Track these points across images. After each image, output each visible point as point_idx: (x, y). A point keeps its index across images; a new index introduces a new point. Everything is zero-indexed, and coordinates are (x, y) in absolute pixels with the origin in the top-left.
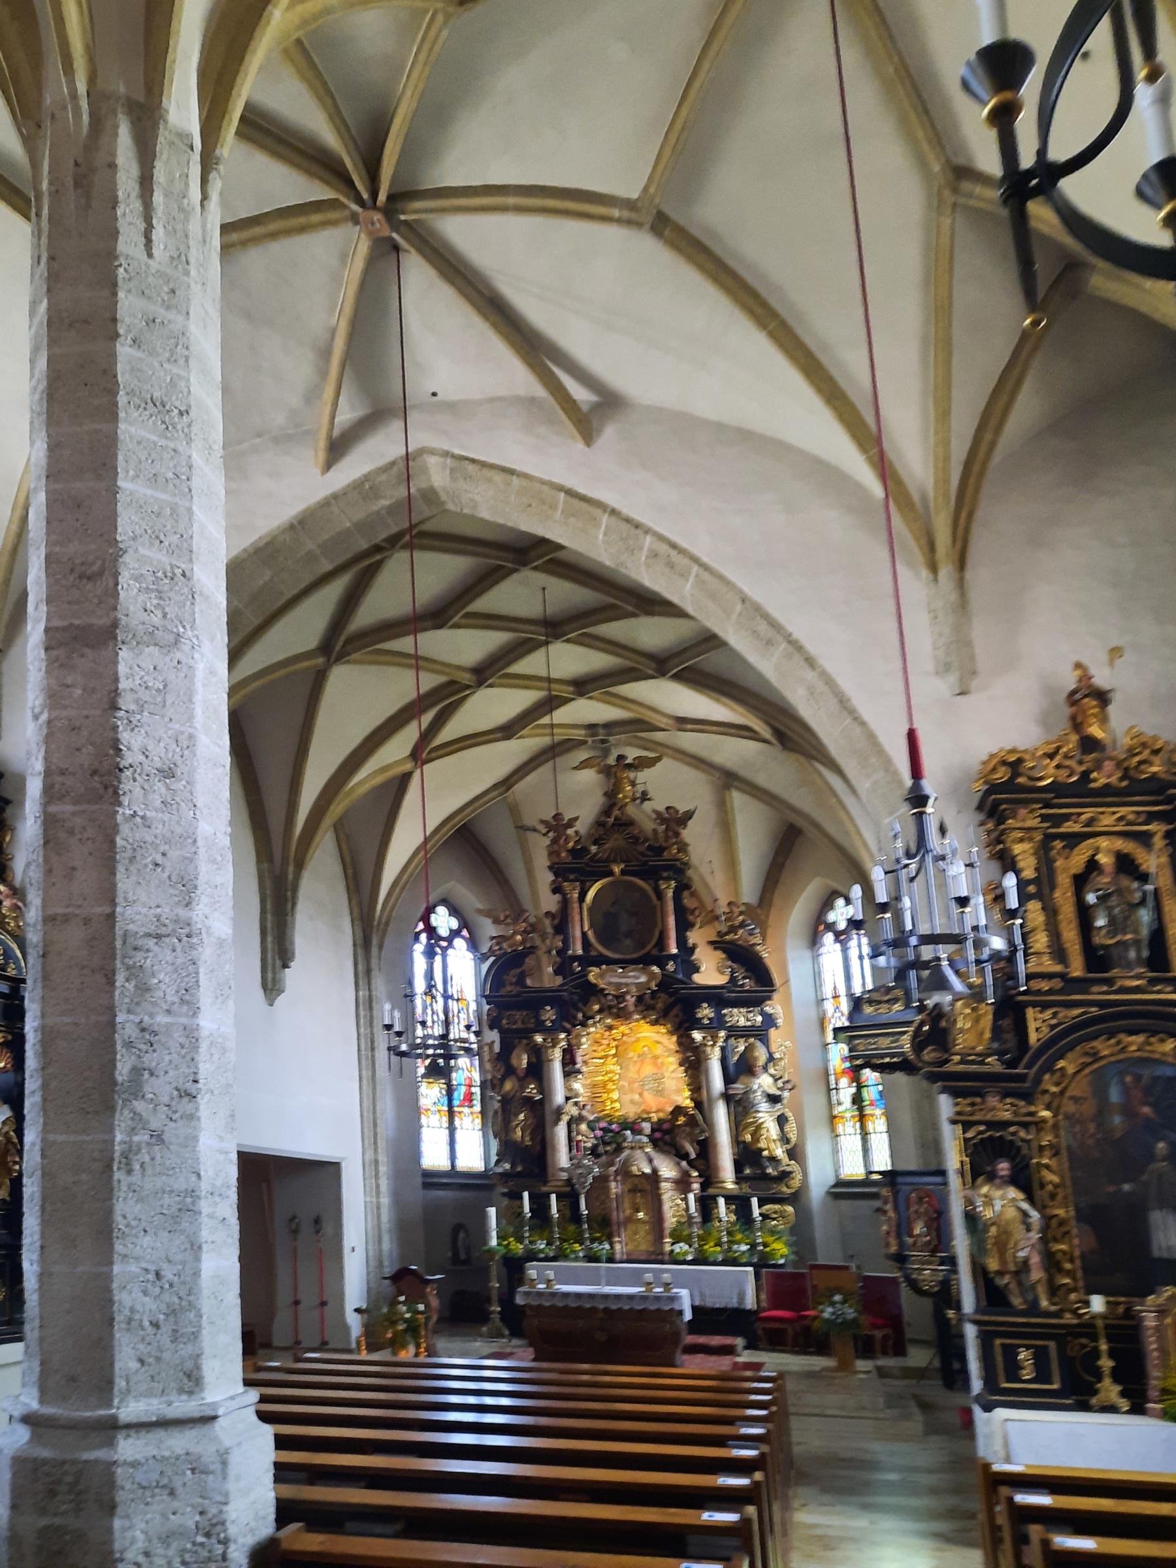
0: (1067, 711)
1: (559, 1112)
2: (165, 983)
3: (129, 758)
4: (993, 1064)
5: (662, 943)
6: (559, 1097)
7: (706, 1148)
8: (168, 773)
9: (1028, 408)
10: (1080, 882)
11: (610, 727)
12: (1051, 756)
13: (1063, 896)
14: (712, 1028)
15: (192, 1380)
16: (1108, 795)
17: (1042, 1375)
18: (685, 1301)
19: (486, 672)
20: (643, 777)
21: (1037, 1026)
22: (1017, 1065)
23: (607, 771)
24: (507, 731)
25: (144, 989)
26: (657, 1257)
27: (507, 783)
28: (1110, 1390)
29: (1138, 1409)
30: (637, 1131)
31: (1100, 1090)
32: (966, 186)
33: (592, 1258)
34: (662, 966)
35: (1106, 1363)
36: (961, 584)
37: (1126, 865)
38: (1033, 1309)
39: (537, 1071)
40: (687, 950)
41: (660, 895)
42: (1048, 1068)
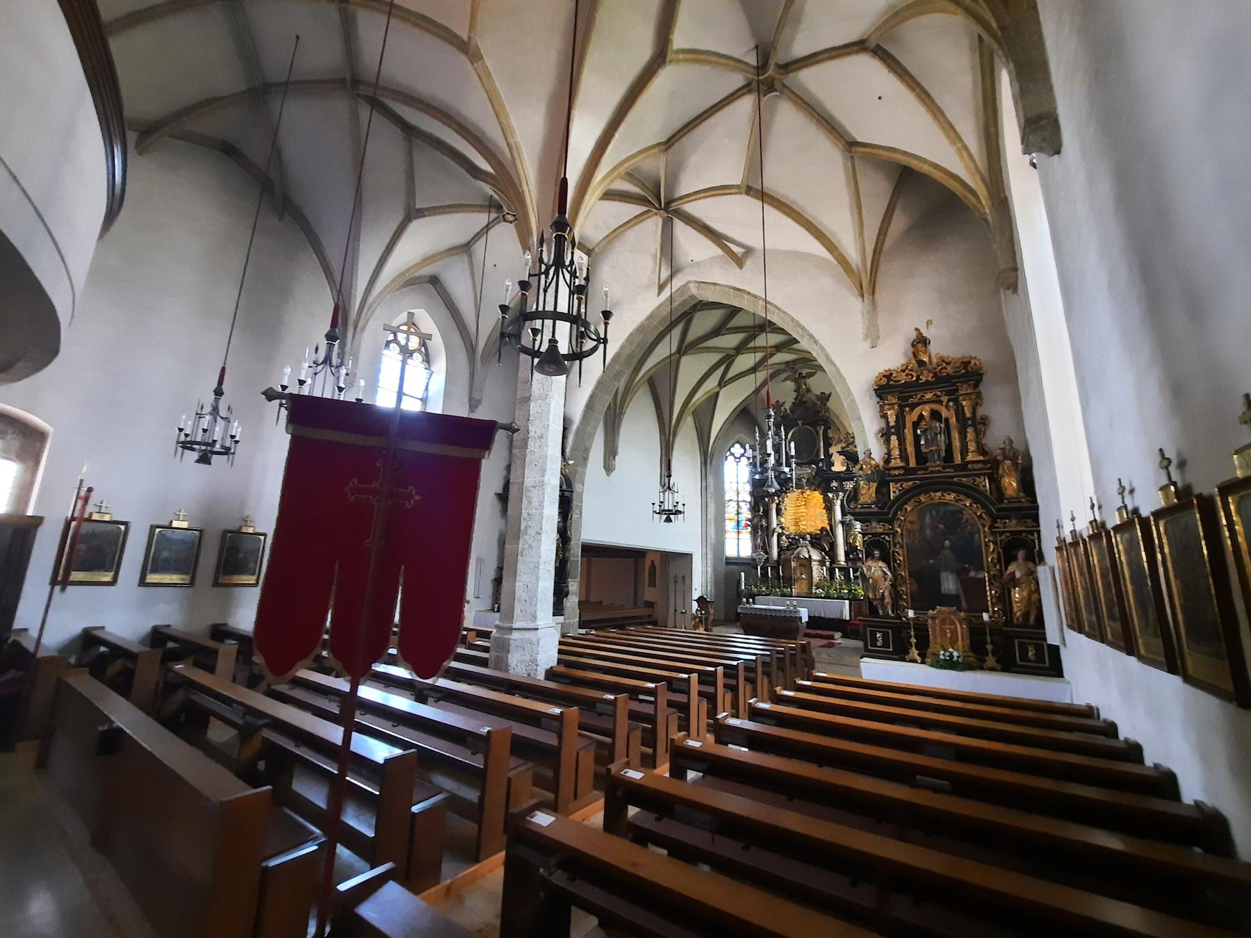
0: (911, 349)
1: (774, 531)
2: (535, 502)
3: (531, 434)
4: (874, 508)
5: (818, 455)
6: (774, 525)
7: (833, 546)
8: (541, 437)
9: (899, 223)
10: (916, 425)
11: (794, 361)
12: (903, 371)
13: (908, 433)
14: (836, 491)
15: (534, 617)
16: (928, 386)
17: (886, 644)
18: (804, 614)
19: (740, 349)
20: (810, 381)
21: (894, 490)
22: (884, 511)
23: (795, 381)
24: (753, 370)
25: (530, 502)
26: (810, 595)
27: (757, 391)
28: (914, 653)
29: (923, 662)
30: (804, 539)
31: (922, 519)
32: (854, 149)
33: (783, 595)
34: (817, 465)
35: (913, 640)
36: (873, 302)
37: (935, 415)
38: (887, 616)
39: (767, 514)
40: (828, 456)
41: (817, 433)
42: (900, 508)
